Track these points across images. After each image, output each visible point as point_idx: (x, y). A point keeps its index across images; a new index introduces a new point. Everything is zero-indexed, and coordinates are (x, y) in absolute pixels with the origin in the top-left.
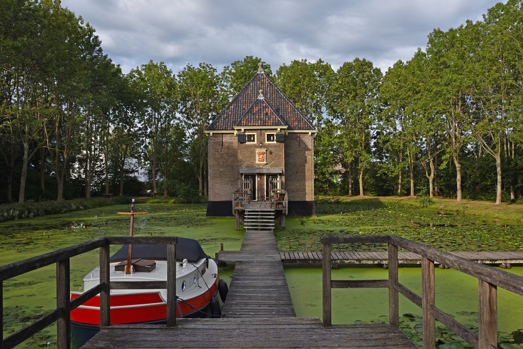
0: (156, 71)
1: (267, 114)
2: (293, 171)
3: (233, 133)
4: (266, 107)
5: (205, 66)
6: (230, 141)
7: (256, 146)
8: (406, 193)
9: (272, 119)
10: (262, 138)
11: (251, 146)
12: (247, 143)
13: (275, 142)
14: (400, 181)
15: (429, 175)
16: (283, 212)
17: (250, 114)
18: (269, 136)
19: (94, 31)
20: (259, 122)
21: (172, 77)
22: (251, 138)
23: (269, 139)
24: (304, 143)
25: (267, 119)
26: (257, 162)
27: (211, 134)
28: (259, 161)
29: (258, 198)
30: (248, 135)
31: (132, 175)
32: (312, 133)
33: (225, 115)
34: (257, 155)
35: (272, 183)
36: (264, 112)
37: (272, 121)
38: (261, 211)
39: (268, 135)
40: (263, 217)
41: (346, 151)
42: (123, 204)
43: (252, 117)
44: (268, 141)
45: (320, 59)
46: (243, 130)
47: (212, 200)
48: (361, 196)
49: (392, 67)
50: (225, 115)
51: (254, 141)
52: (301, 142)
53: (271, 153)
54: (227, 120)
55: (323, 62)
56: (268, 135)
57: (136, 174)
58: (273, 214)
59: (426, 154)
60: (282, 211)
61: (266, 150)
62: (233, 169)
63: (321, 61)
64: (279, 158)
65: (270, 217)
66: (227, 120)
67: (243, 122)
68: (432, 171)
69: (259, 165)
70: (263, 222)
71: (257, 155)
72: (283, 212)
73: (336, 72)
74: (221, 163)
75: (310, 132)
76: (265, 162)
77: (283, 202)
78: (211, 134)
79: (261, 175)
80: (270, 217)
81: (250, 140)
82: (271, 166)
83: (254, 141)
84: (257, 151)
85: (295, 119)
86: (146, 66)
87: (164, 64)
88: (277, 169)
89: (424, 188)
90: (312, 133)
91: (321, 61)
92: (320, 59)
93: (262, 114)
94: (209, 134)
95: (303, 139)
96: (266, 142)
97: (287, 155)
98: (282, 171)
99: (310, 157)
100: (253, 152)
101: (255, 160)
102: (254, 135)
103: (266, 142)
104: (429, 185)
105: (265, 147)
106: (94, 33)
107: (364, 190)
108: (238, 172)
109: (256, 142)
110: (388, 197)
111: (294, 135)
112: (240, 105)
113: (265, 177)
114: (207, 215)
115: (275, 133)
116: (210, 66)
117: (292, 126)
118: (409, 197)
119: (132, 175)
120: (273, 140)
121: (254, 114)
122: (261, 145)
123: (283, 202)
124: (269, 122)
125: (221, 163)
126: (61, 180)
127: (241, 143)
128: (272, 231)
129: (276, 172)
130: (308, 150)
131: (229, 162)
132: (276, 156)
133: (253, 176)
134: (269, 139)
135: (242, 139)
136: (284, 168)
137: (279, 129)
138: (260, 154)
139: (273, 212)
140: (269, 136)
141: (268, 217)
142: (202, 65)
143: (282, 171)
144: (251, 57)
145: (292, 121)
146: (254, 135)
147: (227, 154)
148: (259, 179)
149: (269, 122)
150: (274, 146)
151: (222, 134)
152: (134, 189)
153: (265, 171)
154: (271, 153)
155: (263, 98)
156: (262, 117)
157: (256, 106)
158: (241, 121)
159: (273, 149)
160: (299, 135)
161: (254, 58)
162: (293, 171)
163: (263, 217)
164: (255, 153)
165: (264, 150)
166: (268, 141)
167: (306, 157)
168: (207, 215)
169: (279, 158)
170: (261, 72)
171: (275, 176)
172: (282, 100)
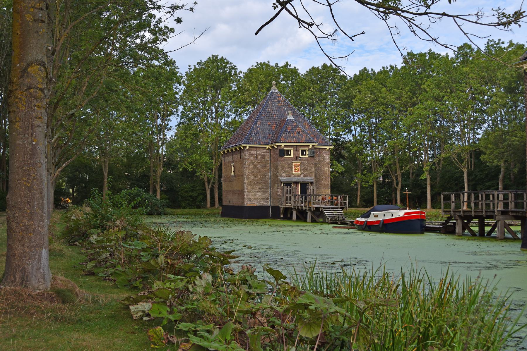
7: (292, 159)
11: (289, 159)
12: (285, 157)
13: (307, 156)
18: (303, 151)
22: (288, 153)
23: (302, 154)
27: (248, 147)
45: (287, 63)
46: (283, 146)
47: (248, 205)
51: (290, 155)
55: (290, 65)
62: (265, 178)
68: (400, 180)
69: (295, 175)
74: (255, 173)
78: (248, 147)
81: (288, 155)
82: (305, 176)
83: (290, 155)
91: (287, 64)
92: (287, 63)
101: (292, 171)
102: (290, 150)
104: (397, 194)
109: (292, 156)
120: (305, 155)
122: (297, 158)
125: (255, 173)
126: (208, 186)
134: (302, 154)
137: (311, 146)
144: (217, 56)
146: (290, 150)
150: (307, 159)
161: (219, 57)
164: (292, 165)
165: (299, 163)
170: (275, 90)
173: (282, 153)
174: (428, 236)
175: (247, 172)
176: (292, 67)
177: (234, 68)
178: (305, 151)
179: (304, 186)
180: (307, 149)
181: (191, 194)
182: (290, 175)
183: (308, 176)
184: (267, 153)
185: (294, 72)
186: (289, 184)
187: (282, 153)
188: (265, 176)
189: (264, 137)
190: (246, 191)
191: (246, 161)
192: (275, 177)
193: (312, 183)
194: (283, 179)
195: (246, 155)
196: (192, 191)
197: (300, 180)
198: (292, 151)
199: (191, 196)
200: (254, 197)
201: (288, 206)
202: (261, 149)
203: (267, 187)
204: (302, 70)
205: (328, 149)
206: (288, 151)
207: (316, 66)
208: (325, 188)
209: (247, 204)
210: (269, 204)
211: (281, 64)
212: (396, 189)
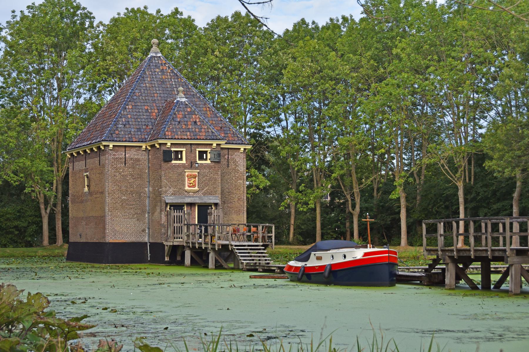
3: (141, 147)
6: (136, 157)
7: (183, 166)
8: (302, 239)
10: (193, 155)
11: (179, 166)
12: (173, 162)
13: (208, 162)
18: (201, 153)
22: (178, 155)
23: (201, 158)
26: (187, 188)
27: (111, 146)
34: (186, 178)
39: (199, 151)
44: (200, 159)
45: (176, 9)
46: (169, 144)
47: (111, 241)
51: (181, 159)
55: (181, 14)
56: (199, 151)
59: (367, 209)
63: (177, 12)
64: (214, 183)
69: (188, 192)
71: (186, 178)
74: (124, 188)
78: (111, 146)
81: (177, 159)
82: (204, 194)
83: (181, 159)
84: (187, 174)
90: (245, 149)
91: (177, 12)
92: (176, 9)
100: (182, 175)
102: (181, 152)
109: (184, 161)
120: (206, 159)
122: (192, 165)
125: (124, 188)
131: (135, 186)
134: (201, 158)
137: (215, 145)
138: (191, 177)
140: (201, 153)
146: (181, 152)
147: (132, 175)
150: (208, 166)
151: (125, 146)
164: (184, 175)
165: (195, 172)
166: (200, 159)
169: (214, 183)
170: (156, 53)
173: (168, 156)
174: (401, 289)
175: (109, 186)
176: (185, 16)
177: (88, 16)
178: (206, 152)
179: (204, 210)
180: (209, 150)
181: (16, 223)
182: (181, 191)
183: (210, 194)
184: (142, 156)
185: (189, 24)
186: (178, 207)
187: (168, 156)
188: (139, 194)
189: (139, 130)
190: (108, 218)
191: (109, 170)
192: (157, 195)
193: (216, 205)
194: (170, 199)
195: (108, 159)
196: (19, 218)
197: (198, 201)
199: (16, 227)
200: (122, 229)
201: (177, 242)
202: (133, 150)
203: (143, 212)
204: (201, 22)
205: (242, 149)
206: (177, 152)
207: (223, 16)
208: (238, 212)
209: (110, 239)
210: (146, 240)
211: (166, 11)
212: (352, 214)
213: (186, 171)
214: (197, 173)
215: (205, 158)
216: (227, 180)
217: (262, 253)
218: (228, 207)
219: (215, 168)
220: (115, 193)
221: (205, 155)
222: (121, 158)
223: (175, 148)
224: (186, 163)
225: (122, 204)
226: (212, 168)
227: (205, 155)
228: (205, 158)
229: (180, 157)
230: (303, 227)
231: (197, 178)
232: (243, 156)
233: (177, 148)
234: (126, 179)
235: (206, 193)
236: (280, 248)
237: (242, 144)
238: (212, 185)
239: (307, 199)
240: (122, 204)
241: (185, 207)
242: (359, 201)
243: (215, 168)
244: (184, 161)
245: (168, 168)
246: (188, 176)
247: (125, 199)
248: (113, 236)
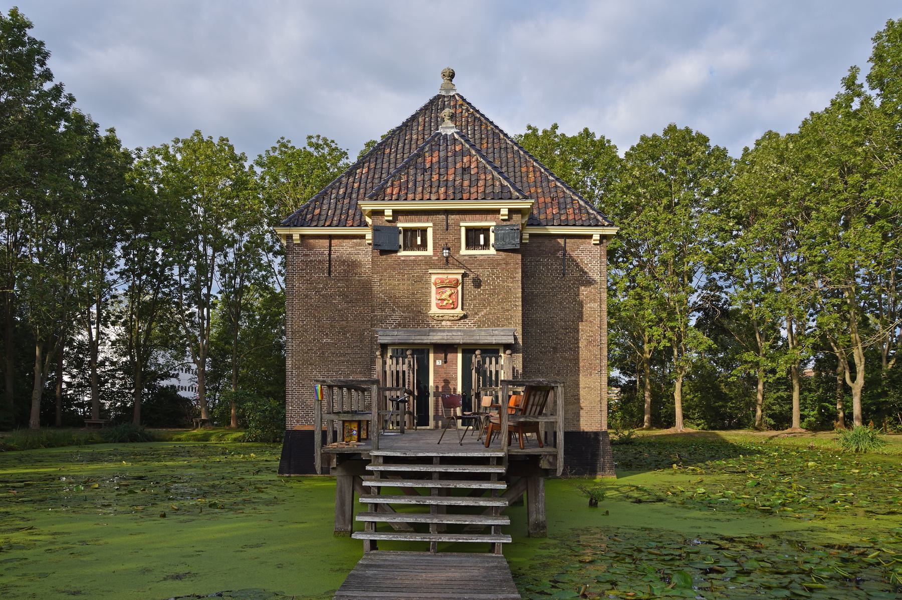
0: (207, 155)
1: (465, 170)
2: (547, 341)
4: (463, 153)
5: (320, 142)
7: (428, 263)
8: (773, 422)
9: (481, 183)
10: (451, 237)
11: (416, 262)
12: (402, 253)
13: (492, 251)
14: (760, 397)
15: (853, 379)
16: (544, 465)
17: (412, 172)
19: (30, 26)
20: (442, 190)
21: (247, 169)
22: (413, 238)
23: (472, 242)
24: (577, 265)
25: (466, 183)
27: (296, 237)
28: (441, 308)
29: (436, 418)
30: (406, 230)
31: (164, 383)
32: (603, 237)
33: (341, 191)
35: (481, 371)
36: (458, 166)
37: (481, 190)
38: (444, 461)
39: (468, 230)
40: (452, 484)
41: (651, 327)
42: (121, 441)
43: (420, 178)
44: (468, 246)
45: (586, 130)
46: (389, 212)
47: (298, 427)
48: (679, 427)
49: (752, 147)
50: (341, 191)
52: (568, 263)
53: (477, 283)
54: (346, 201)
56: (468, 230)
57: (173, 382)
58: (501, 470)
60: (536, 458)
61: (464, 275)
64: (505, 300)
65: (485, 486)
66: (346, 201)
67: (389, 191)
69: (441, 319)
70: (449, 492)
72: (544, 465)
73: (621, 155)
74: (325, 321)
75: (596, 233)
76: (459, 311)
77: (542, 420)
78: (296, 237)
79: (445, 349)
80: (485, 486)
81: (410, 245)
82: (480, 324)
83: (424, 246)
84: (433, 278)
85: (548, 200)
86: (184, 142)
87: (230, 143)
88: (497, 331)
89: (812, 413)
90: (603, 237)
92: (586, 130)
93: (451, 171)
94: (289, 237)
95: (574, 254)
96: (464, 251)
97: (527, 300)
98: (516, 339)
99: (595, 305)
100: (422, 281)
101: (428, 304)
102: (424, 231)
103: (464, 251)
105: (460, 264)
106: (28, 31)
107: (685, 416)
108: (373, 339)
109: (430, 251)
110: (741, 432)
111: (547, 242)
112: (385, 166)
113: (460, 356)
114: (281, 471)
115: (491, 224)
116: (333, 146)
117: (542, 217)
118: (789, 430)
119: (164, 383)
120: (486, 245)
121: (425, 170)
123: (542, 420)
124: (473, 190)
125: (325, 321)
127: (383, 252)
128: (498, 554)
129: (493, 340)
130: (589, 282)
131: (351, 318)
132: (493, 293)
133: (421, 352)
134: (472, 242)
135: (386, 243)
136: (519, 329)
137: (504, 211)
138: (442, 286)
139: (499, 461)
141: (475, 485)
142: (314, 140)
143: (516, 339)
145: (542, 206)
147: (344, 295)
148: (439, 363)
149: (473, 190)
152: (168, 411)
153: (458, 339)
154: (477, 283)
155: (455, 130)
156: (451, 178)
157: (431, 150)
158: (383, 189)
159: (484, 273)
160: (561, 241)
162: (547, 341)
163: (452, 484)
164: (428, 282)
165: (456, 275)
166: (468, 246)
167: (581, 304)
168: (281, 471)
171: (491, 350)
172: (510, 156)
176: (597, 137)
178: (486, 231)
180: (491, 224)
183: (496, 323)
185: (603, 147)
198: (430, 232)
202: (346, 243)
205: (596, 237)
206: (410, 233)
212: (848, 390)
213: (430, 271)
214: (460, 277)
215: (482, 242)
216: (561, 303)
217: (387, 528)
218: (565, 359)
219: (507, 264)
220: (306, 331)
221: (482, 236)
222: (320, 262)
223: (406, 221)
224: (435, 255)
225: (323, 353)
226: (499, 264)
227: (482, 236)
228: (482, 242)
229: (419, 242)
230: (774, 407)
231: (460, 288)
232: (599, 252)
233: (412, 221)
234: (332, 303)
235: (484, 323)
236: (737, 435)
237: (597, 225)
238: (499, 303)
239: (774, 365)
240: (323, 353)
241: (431, 356)
242: (862, 367)
243: (507, 264)
244: (430, 251)
245: (390, 266)
246: (435, 284)
247: (328, 344)
248: (302, 417)
